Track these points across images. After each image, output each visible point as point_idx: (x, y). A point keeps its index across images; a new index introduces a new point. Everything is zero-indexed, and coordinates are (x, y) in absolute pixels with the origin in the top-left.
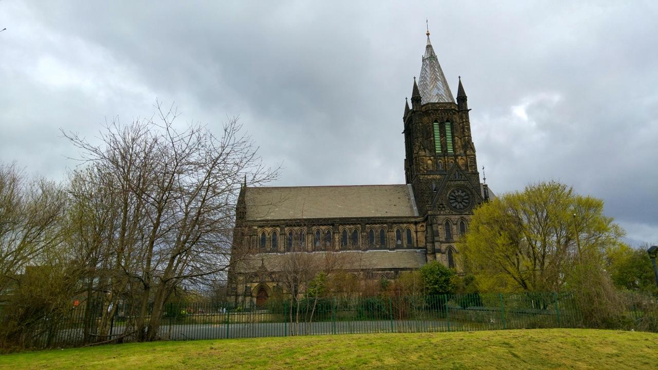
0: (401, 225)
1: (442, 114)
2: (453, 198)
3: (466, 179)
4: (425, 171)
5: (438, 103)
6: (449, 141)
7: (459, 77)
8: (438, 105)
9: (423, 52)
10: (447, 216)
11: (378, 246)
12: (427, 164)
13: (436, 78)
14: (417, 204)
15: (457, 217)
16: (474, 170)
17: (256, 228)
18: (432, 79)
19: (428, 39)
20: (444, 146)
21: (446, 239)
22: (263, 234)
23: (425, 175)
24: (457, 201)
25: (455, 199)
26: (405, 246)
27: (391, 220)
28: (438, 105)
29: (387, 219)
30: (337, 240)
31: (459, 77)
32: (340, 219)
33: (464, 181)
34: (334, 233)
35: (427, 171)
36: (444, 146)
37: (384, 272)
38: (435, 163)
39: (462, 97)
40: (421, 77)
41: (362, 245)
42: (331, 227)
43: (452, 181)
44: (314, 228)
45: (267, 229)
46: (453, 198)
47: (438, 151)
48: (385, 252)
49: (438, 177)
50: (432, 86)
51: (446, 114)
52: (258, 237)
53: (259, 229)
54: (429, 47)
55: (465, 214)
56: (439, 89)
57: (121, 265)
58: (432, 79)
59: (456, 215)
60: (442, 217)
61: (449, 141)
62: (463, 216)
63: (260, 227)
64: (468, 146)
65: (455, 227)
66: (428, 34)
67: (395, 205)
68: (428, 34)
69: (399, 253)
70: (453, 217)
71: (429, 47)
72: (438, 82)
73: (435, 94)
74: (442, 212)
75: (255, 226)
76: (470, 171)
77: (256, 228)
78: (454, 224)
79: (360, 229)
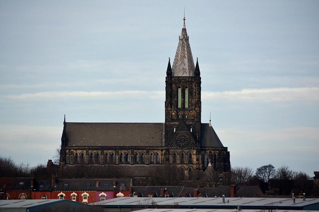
0: (154, 151)
1: (183, 84)
2: (179, 140)
3: (187, 130)
4: (170, 120)
5: (181, 77)
9: (180, 33)
10: (175, 150)
11: (140, 163)
12: (172, 115)
13: (184, 56)
14: (166, 138)
15: (180, 150)
16: (198, 120)
17: (72, 150)
18: (181, 57)
19: (184, 22)
22: (77, 154)
23: (170, 122)
24: (181, 142)
25: (181, 141)
26: (155, 163)
28: (181, 78)
29: (145, 148)
30: (117, 159)
32: (120, 206)
33: (186, 130)
35: (171, 119)
37: (140, 178)
38: (177, 115)
41: (131, 162)
43: (180, 130)
46: (179, 140)
47: (180, 106)
49: (177, 123)
50: (181, 62)
51: (186, 84)
52: (74, 155)
53: (74, 151)
54: (184, 30)
55: (184, 149)
56: (185, 65)
58: (181, 57)
59: (179, 149)
62: (183, 150)
63: (74, 150)
64: (198, 103)
65: (178, 156)
66: (184, 20)
67: (152, 138)
69: (151, 167)
70: (178, 150)
71: (184, 30)
72: (185, 59)
73: (182, 69)
74: (172, 148)
75: (72, 149)
76: (196, 120)
77: (72, 150)
78: (178, 154)
79: (131, 152)
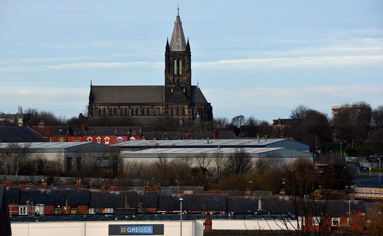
6: (181, 69)
7: (188, 38)
8: (176, 53)
11: (147, 115)
13: (179, 36)
20: (178, 71)
21: (177, 114)
22: (100, 109)
27: (153, 104)
30: (130, 112)
31: (188, 38)
34: (129, 109)
35: (169, 83)
36: (178, 71)
38: (174, 80)
39: (188, 47)
40: (172, 39)
42: (128, 106)
44: (110, 107)
45: (102, 107)
48: (149, 117)
50: (176, 41)
53: (99, 107)
54: (178, 17)
56: (179, 42)
57: (192, 109)
59: (176, 105)
60: (170, 106)
61: (181, 69)
66: (178, 9)
68: (178, 9)
71: (178, 17)
76: (187, 83)
78: (175, 108)
